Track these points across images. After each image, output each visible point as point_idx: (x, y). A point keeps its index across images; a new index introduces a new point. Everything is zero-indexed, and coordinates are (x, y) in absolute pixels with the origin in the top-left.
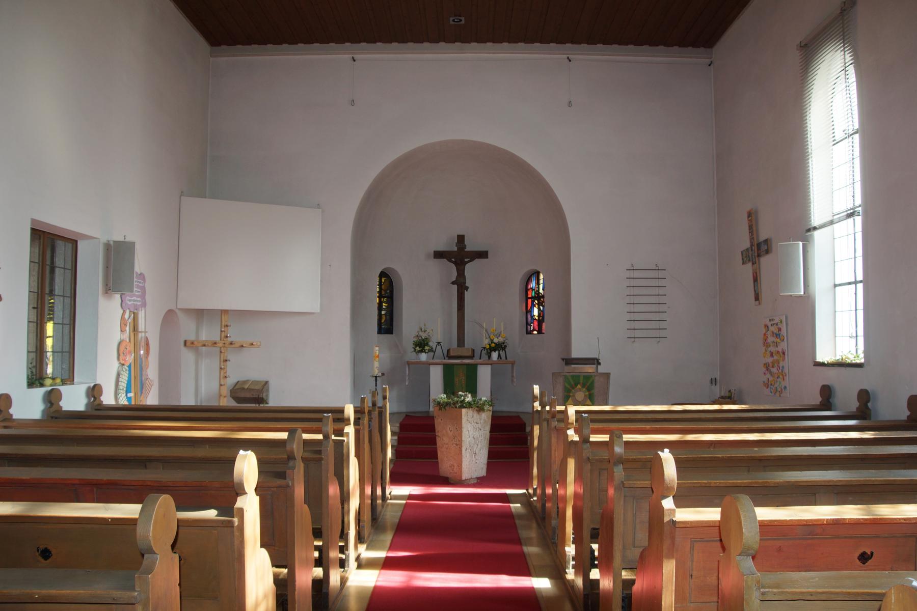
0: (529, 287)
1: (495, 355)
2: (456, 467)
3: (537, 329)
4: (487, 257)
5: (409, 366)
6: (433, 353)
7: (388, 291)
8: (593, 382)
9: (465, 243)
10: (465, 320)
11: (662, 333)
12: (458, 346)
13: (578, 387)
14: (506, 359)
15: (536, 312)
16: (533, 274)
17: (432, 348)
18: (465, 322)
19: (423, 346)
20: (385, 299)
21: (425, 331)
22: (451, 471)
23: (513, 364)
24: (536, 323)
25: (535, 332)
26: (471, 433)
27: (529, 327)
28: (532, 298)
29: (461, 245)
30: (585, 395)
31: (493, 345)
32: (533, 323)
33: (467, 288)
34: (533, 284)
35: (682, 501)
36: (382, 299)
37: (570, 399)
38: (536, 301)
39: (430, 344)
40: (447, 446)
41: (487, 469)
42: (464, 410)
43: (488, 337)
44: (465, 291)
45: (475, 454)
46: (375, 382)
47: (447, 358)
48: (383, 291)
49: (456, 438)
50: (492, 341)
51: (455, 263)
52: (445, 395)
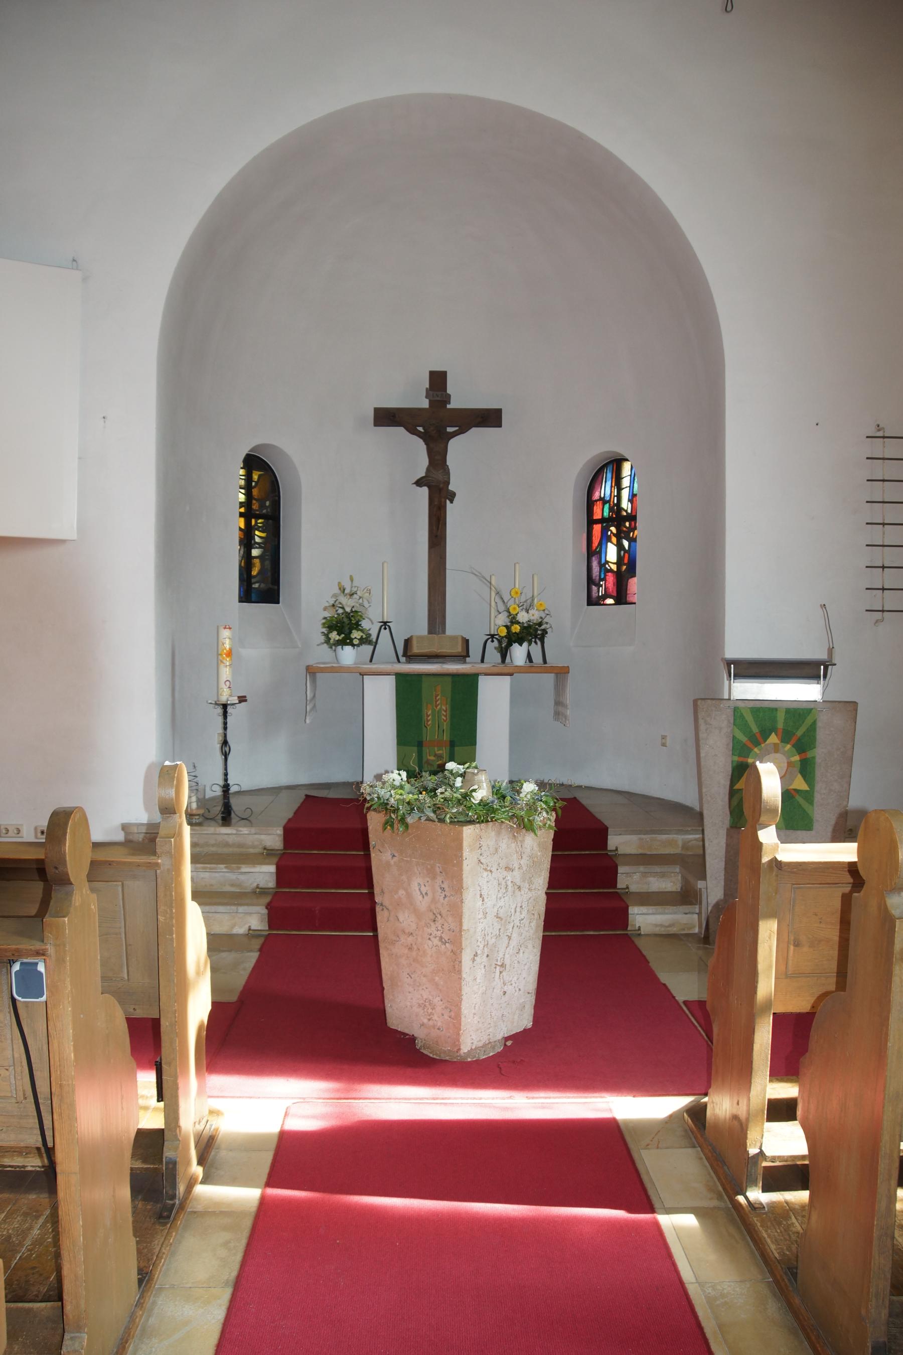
0: (596, 496)
1: (519, 653)
2: (439, 1009)
3: (615, 594)
4: (499, 424)
5: (314, 681)
7: (268, 503)
8: (813, 728)
9: (448, 392)
10: (448, 566)
12: (431, 631)
13: (768, 741)
14: (545, 661)
15: (612, 554)
16: (605, 466)
18: (447, 571)
19: (346, 629)
20: (260, 521)
22: (425, 1021)
23: (561, 673)
24: (611, 578)
25: (610, 601)
26: (489, 903)
27: (594, 588)
28: (602, 520)
29: (439, 393)
30: (790, 764)
31: (516, 628)
32: (604, 579)
33: (452, 496)
34: (606, 489)
38: (613, 529)
39: (365, 624)
40: (410, 939)
41: (536, 1007)
42: (468, 832)
43: (501, 607)
44: (448, 502)
45: (502, 965)
46: (220, 720)
47: (403, 659)
48: (254, 502)
49: (440, 920)
50: (514, 620)
51: (425, 437)
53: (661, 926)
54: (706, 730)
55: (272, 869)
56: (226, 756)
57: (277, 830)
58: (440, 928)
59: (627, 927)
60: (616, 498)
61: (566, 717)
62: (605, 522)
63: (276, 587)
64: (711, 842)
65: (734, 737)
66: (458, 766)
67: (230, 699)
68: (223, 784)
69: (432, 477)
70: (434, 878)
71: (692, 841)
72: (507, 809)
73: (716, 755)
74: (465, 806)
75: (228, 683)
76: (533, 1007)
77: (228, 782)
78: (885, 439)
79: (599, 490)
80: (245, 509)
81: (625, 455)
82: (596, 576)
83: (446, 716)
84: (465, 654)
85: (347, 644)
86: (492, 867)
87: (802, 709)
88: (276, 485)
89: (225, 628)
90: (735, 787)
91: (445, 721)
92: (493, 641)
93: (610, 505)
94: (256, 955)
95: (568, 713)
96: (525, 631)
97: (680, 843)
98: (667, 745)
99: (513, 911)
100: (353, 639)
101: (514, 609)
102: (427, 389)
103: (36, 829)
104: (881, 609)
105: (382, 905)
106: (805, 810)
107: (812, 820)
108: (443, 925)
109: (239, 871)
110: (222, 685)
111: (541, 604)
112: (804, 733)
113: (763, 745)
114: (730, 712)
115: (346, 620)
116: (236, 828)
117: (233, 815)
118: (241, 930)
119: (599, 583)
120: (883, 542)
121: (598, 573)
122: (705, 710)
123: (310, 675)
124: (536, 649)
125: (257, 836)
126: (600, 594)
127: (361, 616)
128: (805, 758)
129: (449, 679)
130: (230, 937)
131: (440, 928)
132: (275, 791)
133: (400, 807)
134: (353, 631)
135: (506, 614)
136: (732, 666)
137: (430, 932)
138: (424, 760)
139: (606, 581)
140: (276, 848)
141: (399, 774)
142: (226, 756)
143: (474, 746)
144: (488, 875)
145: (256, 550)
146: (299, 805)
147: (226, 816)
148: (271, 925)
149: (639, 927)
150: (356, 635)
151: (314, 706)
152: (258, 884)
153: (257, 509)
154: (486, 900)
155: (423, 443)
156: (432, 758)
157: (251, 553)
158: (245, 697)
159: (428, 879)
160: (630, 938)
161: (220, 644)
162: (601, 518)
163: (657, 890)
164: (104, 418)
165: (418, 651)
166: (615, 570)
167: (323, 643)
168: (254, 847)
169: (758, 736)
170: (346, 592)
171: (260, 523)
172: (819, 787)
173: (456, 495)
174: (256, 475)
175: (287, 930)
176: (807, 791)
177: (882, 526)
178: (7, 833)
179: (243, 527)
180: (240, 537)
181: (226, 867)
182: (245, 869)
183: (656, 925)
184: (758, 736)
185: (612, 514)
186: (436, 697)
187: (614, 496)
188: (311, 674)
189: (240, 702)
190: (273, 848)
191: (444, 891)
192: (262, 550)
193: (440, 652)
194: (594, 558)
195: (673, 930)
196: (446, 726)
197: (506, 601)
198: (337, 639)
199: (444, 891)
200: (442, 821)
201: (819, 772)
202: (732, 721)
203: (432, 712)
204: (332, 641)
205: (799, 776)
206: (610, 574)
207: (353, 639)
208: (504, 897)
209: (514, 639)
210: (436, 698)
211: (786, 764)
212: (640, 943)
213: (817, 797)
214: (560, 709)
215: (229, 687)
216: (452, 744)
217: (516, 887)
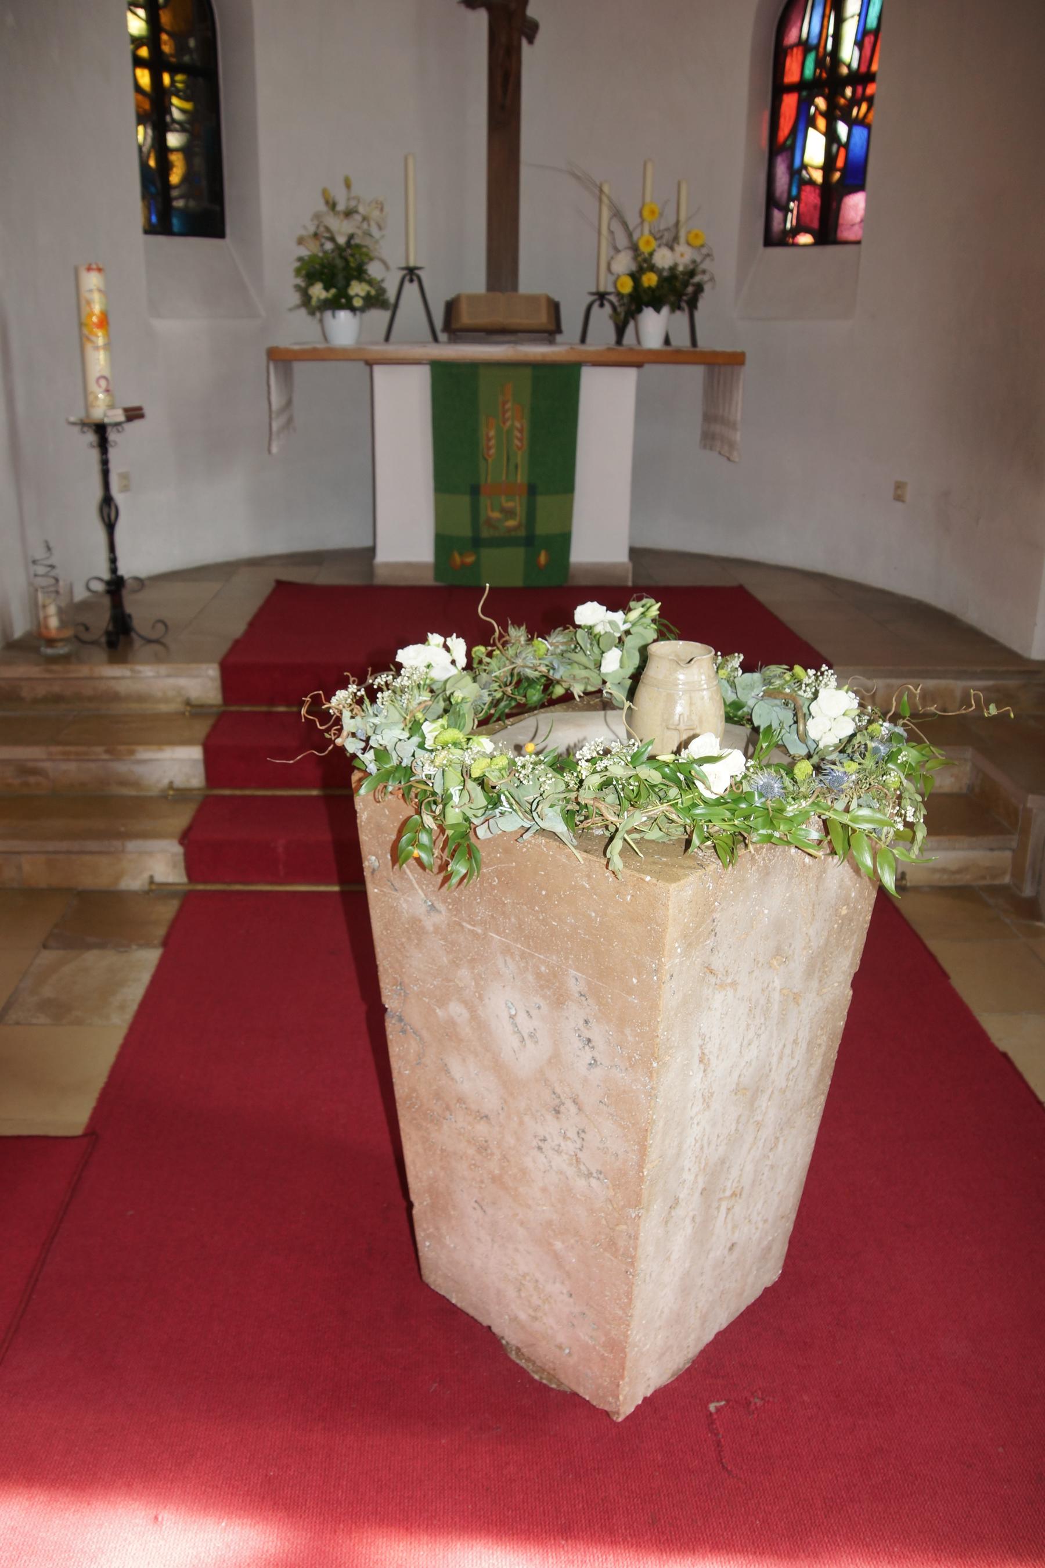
0: (792, 37)
3: (815, 225)
6: (384, 315)
7: (192, 43)
17: (382, 291)
20: (179, 77)
21: (348, 214)
24: (812, 198)
25: (805, 239)
27: (777, 215)
31: (650, 280)
35: (1008, 710)
38: (821, 102)
39: (374, 270)
43: (622, 241)
44: (524, 42)
46: (95, 455)
47: (443, 337)
48: (164, 37)
50: (644, 264)
52: (458, 645)
53: (944, 870)
55: (195, 753)
56: (110, 527)
61: (732, 445)
62: (807, 89)
67: (111, 413)
70: (559, 1001)
74: (674, 805)
75: (103, 383)
76: (787, 1240)
79: (799, 24)
83: (521, 440)
85: (342, 307)
91: (519, 448)
92: (602, 305)
105: (401, 1019)
108: (584, 1131)
110: (93, 386)
115: (340, 263)
116: (129, 666)
119: (788, 204)
123: (276, 368)
126: (788, 226)
127: (367, 255)
129: (528, 372)
131: (572, 1134)
133: (452, 791)
138: (482, 518)
141: (447, 648)
142: (110, 527)
150: (357, 289)
151: (290, 420)
156: (496, 515)
159: (538, 1000)
161: (83, 303)
168: (166, 700)
195: (965, 879)
196: (521, 458)
204: (314, 302)
208: (759, 1035)
214: (717, 428)
216: (532, 491)
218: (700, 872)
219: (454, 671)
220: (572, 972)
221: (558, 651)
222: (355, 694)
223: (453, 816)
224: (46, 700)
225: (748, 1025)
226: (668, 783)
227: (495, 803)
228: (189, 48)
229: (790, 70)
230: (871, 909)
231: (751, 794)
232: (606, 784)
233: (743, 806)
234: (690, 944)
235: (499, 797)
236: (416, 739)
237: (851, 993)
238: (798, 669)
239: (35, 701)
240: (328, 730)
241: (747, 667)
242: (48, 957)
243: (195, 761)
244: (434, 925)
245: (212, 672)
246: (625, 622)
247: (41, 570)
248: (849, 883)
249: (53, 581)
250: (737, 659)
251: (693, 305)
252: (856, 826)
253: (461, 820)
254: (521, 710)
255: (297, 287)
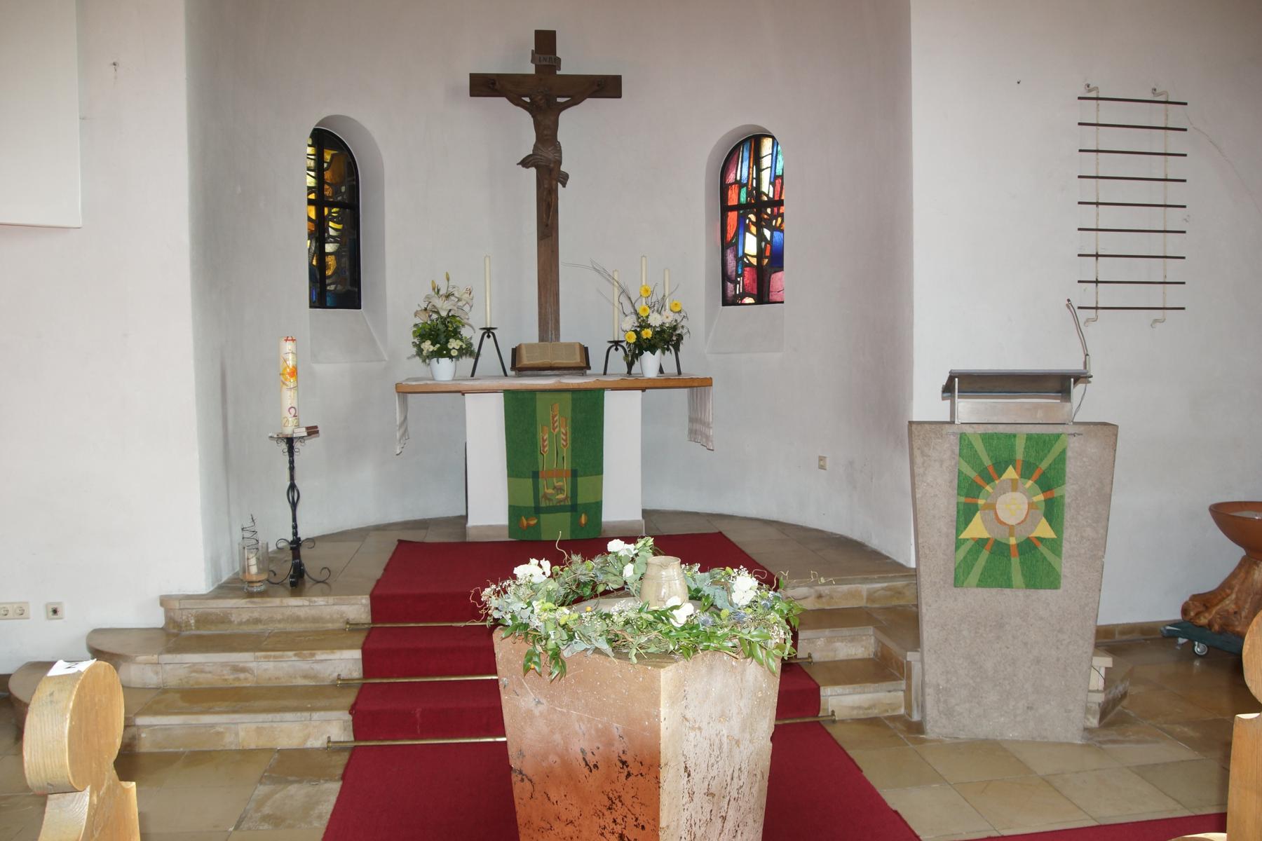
0: (731, 178)
1: (650, 364)
3: (755, 292)
5: (404, 403)
6: (471, 361)
7: (343, 189)
8: (1061, 458)
9: (558, 55)
11: (1173, 296)
12: (542, 339)
13: (1005, 476)
14: (679, 372)
15: (750, 245)
20: (334, 210)
21: (448, 296)
23: (700, 385)
25: (748, 300)
27: (730, 286)
30: (1032, 506)
31: (648, 333)
32: (742, 275)
34: (743, 171)
36: (326, 210)
37: (978, 515)
38: (753, 217)
39: (465, 332)
42: (667, 675)
43: (628, 309)
44: (560, 186)
46: (287, 458)
47: (509, 372)
48: (326, 187)
50: (643, 324)
52: (546, 564)
53: (860, 708)
54: (923, 463)
55: (357, 654)
56: (294, 505)
57: (362, 599)
58: (619, 820)
59: (818, 713)
60: (754, 181)
61: (707, 438)
63: (356, 290)
64: (930, 606)
65: (960, 472)
66: (627, 546)
67: (296, 431)
68: (292, 539)
69: (541, 155)
71: (878, 590)
72: (726, 630)
73: (936, 496)
74: (661, 632)
77: (298, 536)
78: (1099, 102)
79: (734, 172)
80: (315, 196)
81: (771, 131)
82: (732, 272)
83: (565, 440)
84: (585, 365)
85: (443, 356)
86: (701, 721)
87: (1048, 435)
88: (340, 144)
89: (286, 340)
90: (962, 536)
92: (617, 349)
93: (747, 188)
94: (335, 787)
95: (711, 434)
96: (657, 336)
97: (865, 594)
98: (827, 467)
99: (729, 779)
100: (451, 350)
101: (645, 310)
102: (532, 51)
103: (47, 606)
104: (1094, 306)
105: (521, 773)
106: (1050, 564)
107: (1060, 576)
108: (626, 817)
109: (314, 659)
111: (676, 304)
112: (1050, 465)
113: (997, 482)
114: (954, 440)
115: (441, 327)
116: (308, 598)
117: (306, 576)
118: (317, 742)
120: (1097, 225)
121: (735, 268)
122: (921, 437)
124: (670, 357)
125: (336, 607)
126: (738, 293)
127: (460, 322)
128: (1051, 497)
130: (303, 753)
132: (361, 534)
133: (550, 633)
134: (451, 340)
135: (634, 317)
136: (957, 379)
137: (602, 824)
138: (541, 494)
139: (744, 277)
140: (363, 621)
141: (540, 566)
142: (294, 505)
143: (600, 476)
144: (696, 735)
145: (331, 245)
146: (390, 554)
147: (297, 580)
148: (358, 731)
149: (833, 712)
150: (454, 344)
152: (339, 675)
153: (330, 195)
154: (693, 774)
155: (530, 116)
156: (550, 491)
157: (324, 248)
158: (316, 427)
160: (823, 728)
162: (736, 204)
163: (845, 658)
164: (114, 64)
165: (528, 363)
166: (755, 264)
167: (414, 356)
168: (332, 621)
169: (991, 470)
170: (441, 293)
171: (334, 213)
172: (1069, 533)
173: (570, 177)
174: (328, 154)
175: (380, 740)
176: (1053, 539)
177: (1095, 206)
178: (6, 615)
179: (313, 216)
180: (309, 229)
181: (295, 655)
182: (320, 655)
183: (853, 708)
184: (991, 470)
185: (750, 200)
186: (553, 418)
187: (753, 178)
188: (401, 394)
189: (310, 434)
190: (358, 622)
191: (627, 766)
192: (338, 245)
193: (555, 363)
194: (729, 251)
195: (874, 713)
196: (566, 452)
197: (633, 302)
198: (431, 350)
199: (627, 766)
200: (625, 657)
201: (1068, 514)
202: (957, 451)
203: (549, 437)
204: (425, 353)
205: (1044, 520)
206: (747, 269)
207: (451, 350)
208: (717, 762)
209: (645, 346)
210: (553, 419)
211: (1026, 506)
212: (835, 731)
213: (1066, 547)
214: (697, 426)
215: (294, 416)
216: (574, 474)
217: (734, 743)
218: (675, 664)
219: (544, 578)
220: (615, 725)
221: (599, 567)
222: (495, 589)
223: (551, 644)
224: (248, 622)
225: (711, 754)
226: (657, 621)
227: (571, 638)
228: (341, 192)
229: (731, 198)
230: (777, 695)
231: (698, 625)
232: (627, 622)
233: (695, 631)
234: (673, 702)
235: (574, 635)
236: (530, 608)
237: (771, 744)
238: (728, 569)
239: (241, 623)
240: (482, 608)
241: (702, 570)
242: (263, 790)
243: (356, 660)
244: (540, 712)
245: (365, 600)
246: (635, 549)
247: (247, 534)
248: (760, 679)
249: (254, 542)
250: (697, 567)
251: (677, 349)
252: (753, 640)
253: (555, 647)
254: (580, 600)
255: (415, 344)
